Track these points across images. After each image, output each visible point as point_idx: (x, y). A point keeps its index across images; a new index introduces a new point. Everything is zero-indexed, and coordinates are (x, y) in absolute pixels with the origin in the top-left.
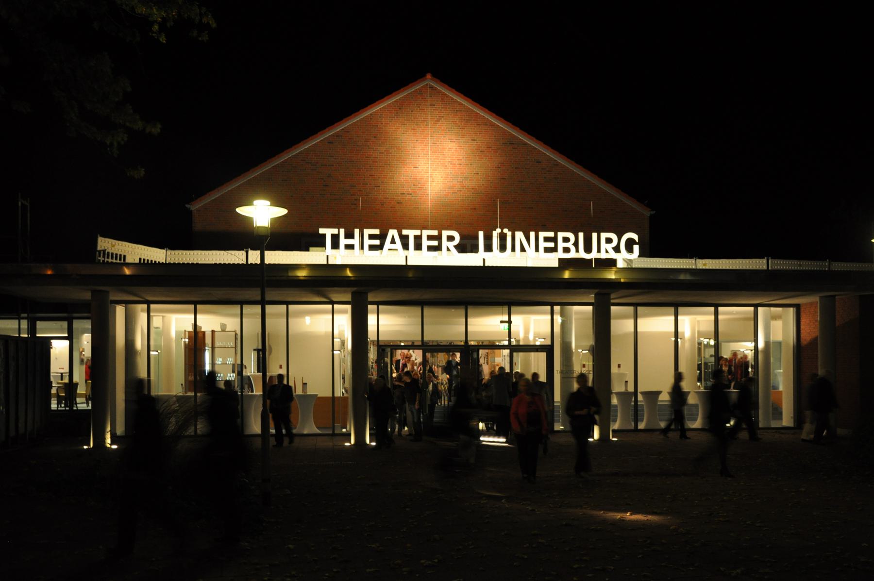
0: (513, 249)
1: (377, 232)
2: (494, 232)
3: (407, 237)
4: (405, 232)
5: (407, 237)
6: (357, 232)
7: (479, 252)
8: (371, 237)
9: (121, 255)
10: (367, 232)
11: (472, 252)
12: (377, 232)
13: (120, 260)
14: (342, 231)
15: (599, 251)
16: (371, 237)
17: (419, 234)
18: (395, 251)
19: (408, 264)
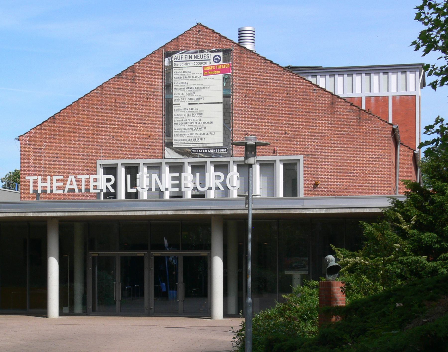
0: (391, 157)
1: (62, 177)
2: (137, 175)
3: (81, 180)
4: (79, 177)
5: (81, 180)
6: (49, 177)
7: (330, 78)
8: (58, 181)
9: (391, 154)
10: (55, 178)
11: (224, 316)
12: (62, 177)
13: (391, 139)
14: (40, 178)
15: (201, 55)
16: (58, 181)
17: (89, 178)
18: (387, 90)
19: (222, 142)
